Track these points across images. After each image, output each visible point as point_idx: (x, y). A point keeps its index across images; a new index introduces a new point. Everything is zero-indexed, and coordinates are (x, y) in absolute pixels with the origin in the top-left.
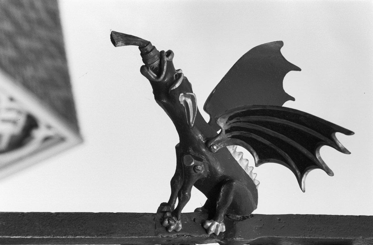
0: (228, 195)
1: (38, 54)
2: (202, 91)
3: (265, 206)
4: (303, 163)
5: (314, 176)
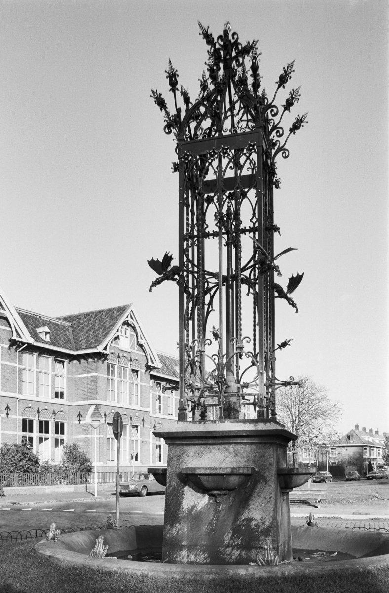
0: (176, 271)
1: (101, 321)
2: (158, 276)
3: (177, 264)
4: (171, 259)
5: (173, 257)
